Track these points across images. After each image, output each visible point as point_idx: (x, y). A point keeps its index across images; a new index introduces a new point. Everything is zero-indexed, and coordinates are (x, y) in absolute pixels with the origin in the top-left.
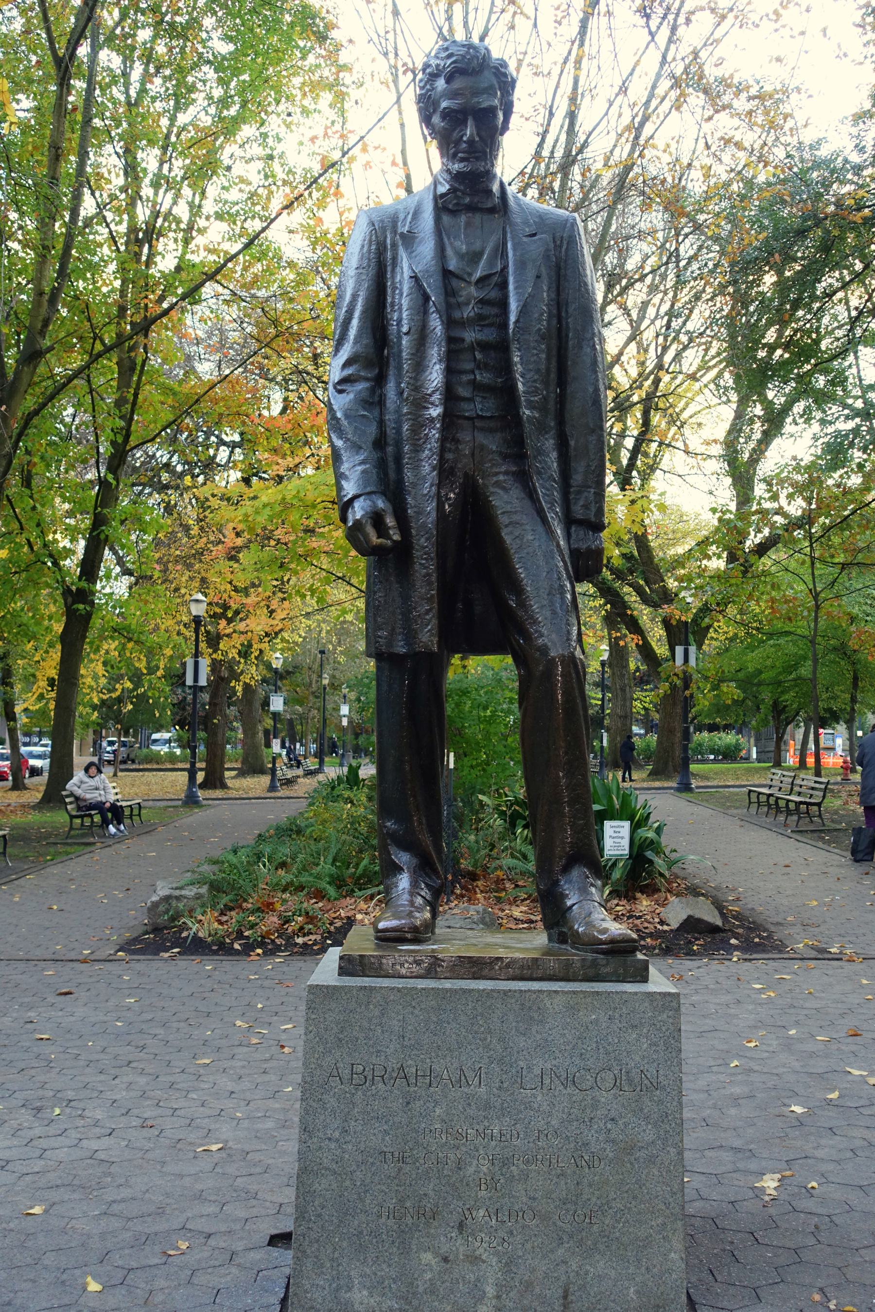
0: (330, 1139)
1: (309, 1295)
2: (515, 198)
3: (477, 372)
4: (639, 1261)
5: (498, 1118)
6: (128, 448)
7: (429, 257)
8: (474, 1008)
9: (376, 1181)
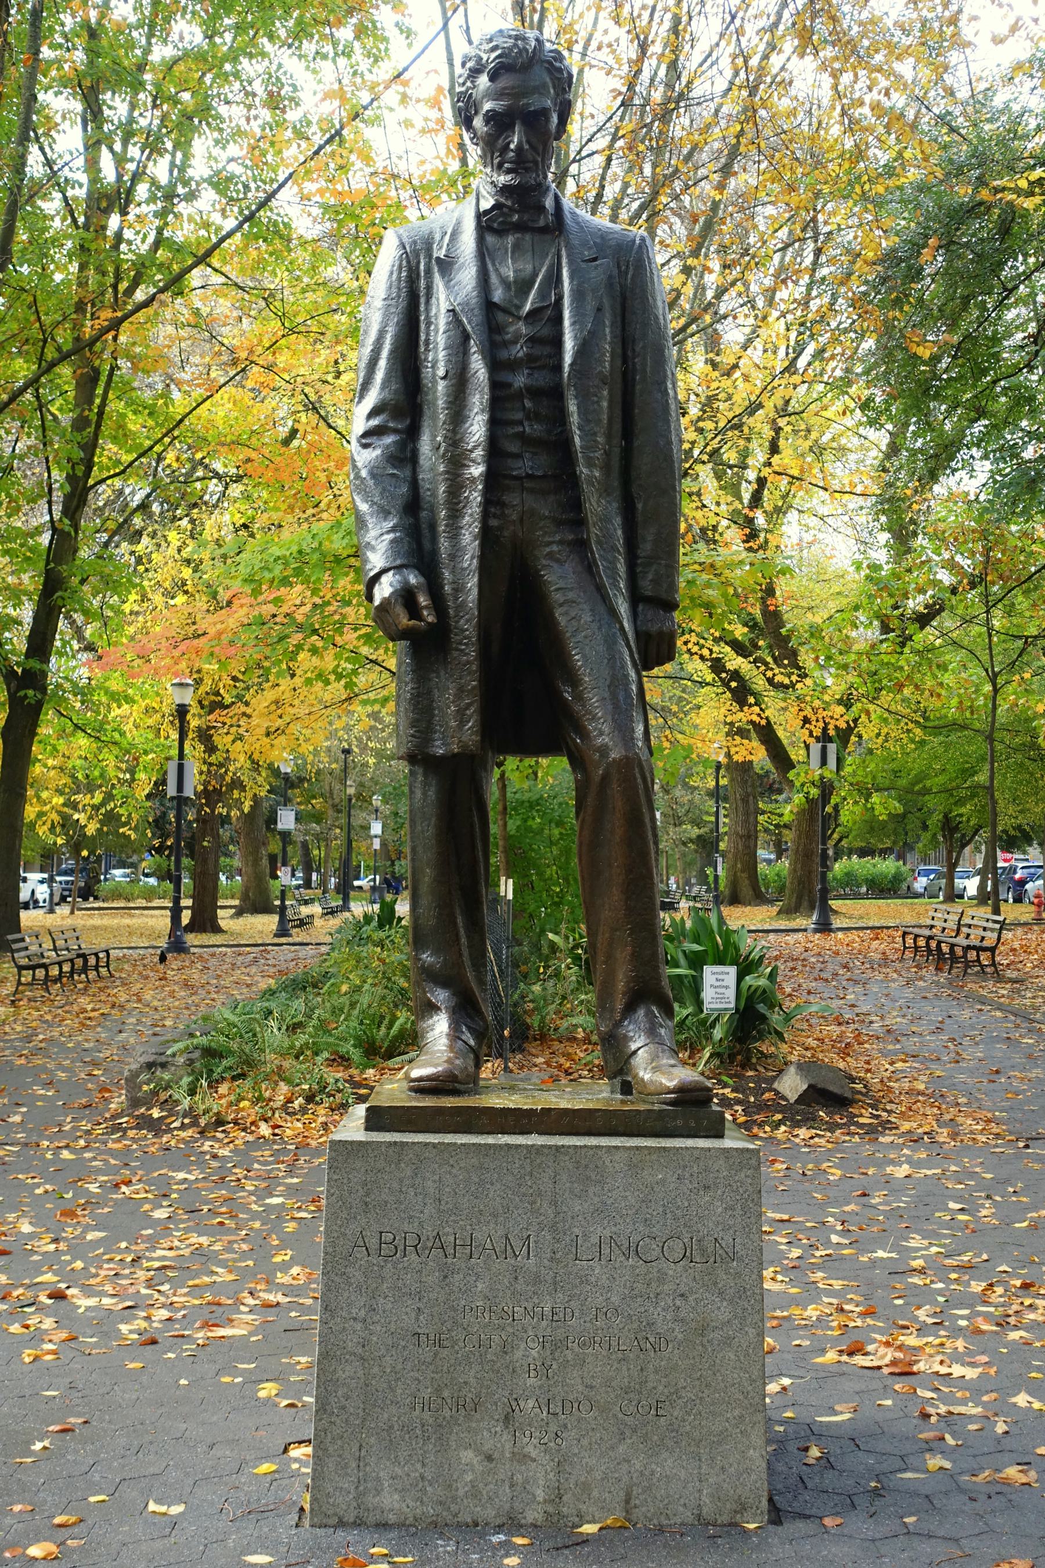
0: (355, 1319)
1: (331, 1501)
2: (573, 214)
3: (526, 424)
4: (712, 1459)
5: (550, 1294)
6: (91, 482)
7: (469, 287)
8: (522, 1167)
9: (409, 1367)
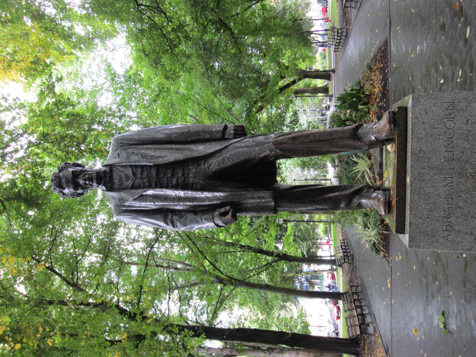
5: (466, 170)
